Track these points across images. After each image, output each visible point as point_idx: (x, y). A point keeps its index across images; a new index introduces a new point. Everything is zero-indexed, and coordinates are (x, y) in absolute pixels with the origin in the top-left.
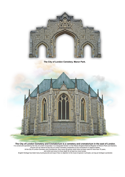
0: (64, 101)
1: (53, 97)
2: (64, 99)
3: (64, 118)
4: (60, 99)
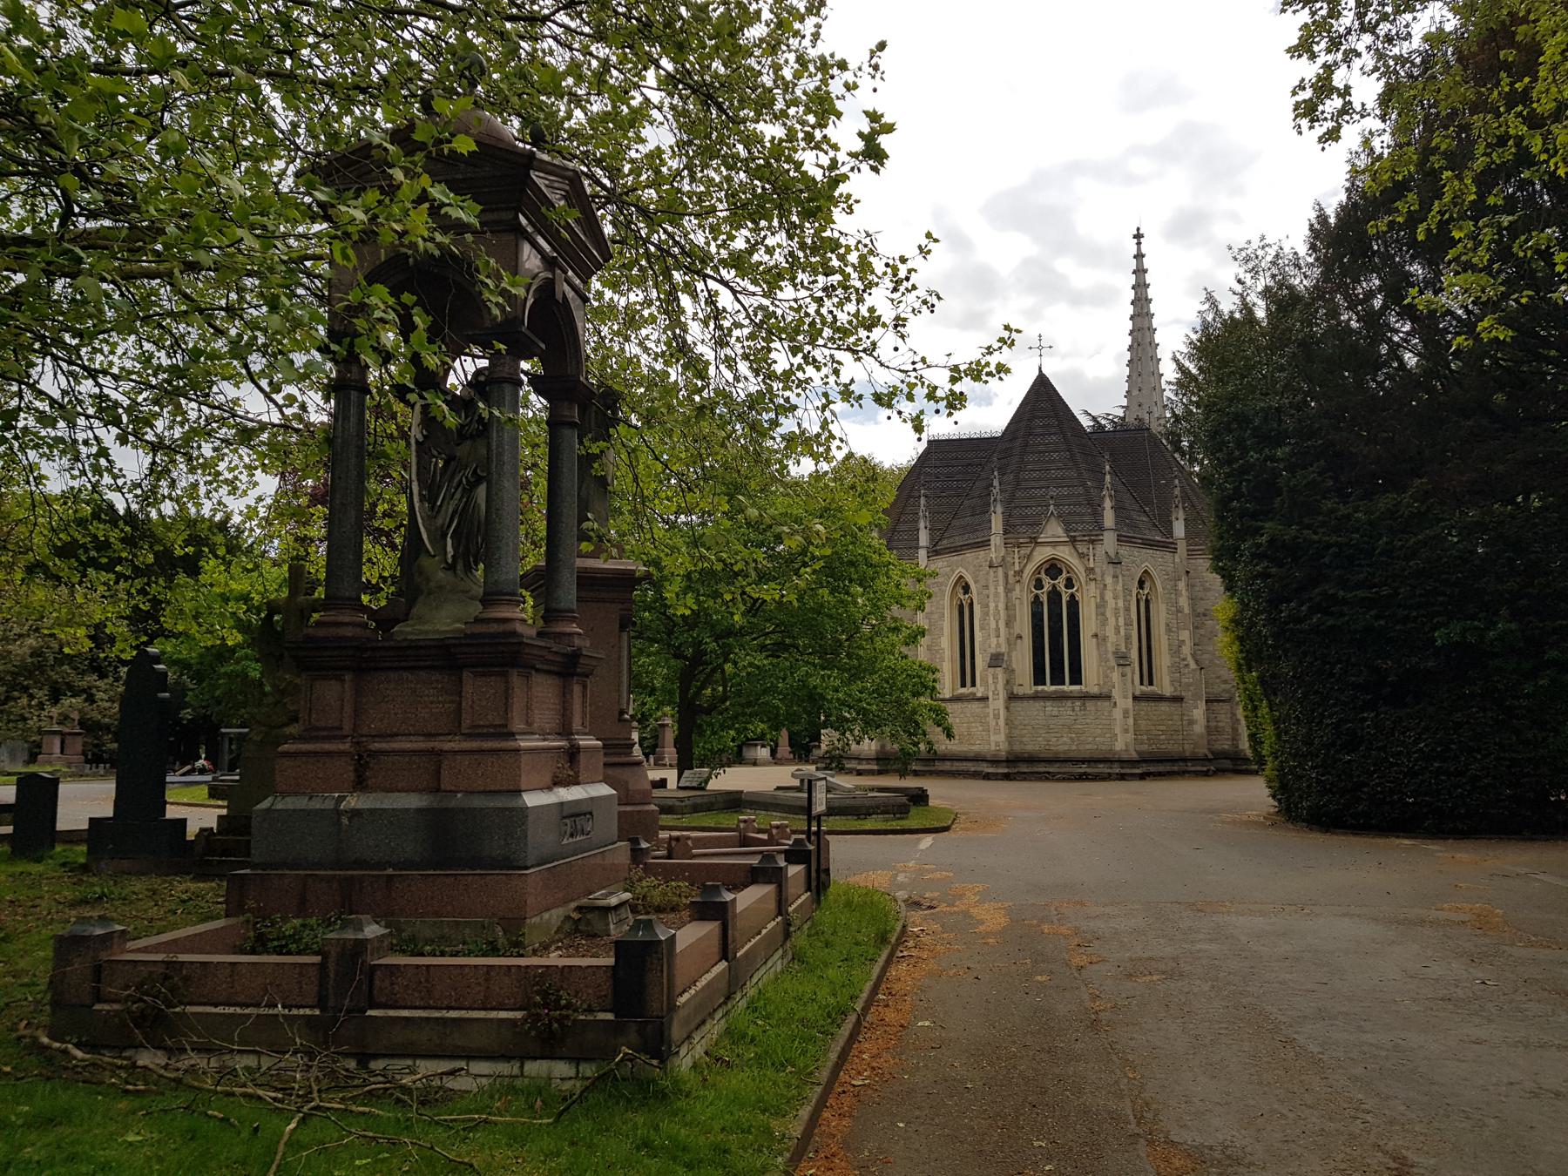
0: (1055, 595)
1: (1006, 576)
2: (1054, 586)
3: (1058, 679)
4: (1039, 585)
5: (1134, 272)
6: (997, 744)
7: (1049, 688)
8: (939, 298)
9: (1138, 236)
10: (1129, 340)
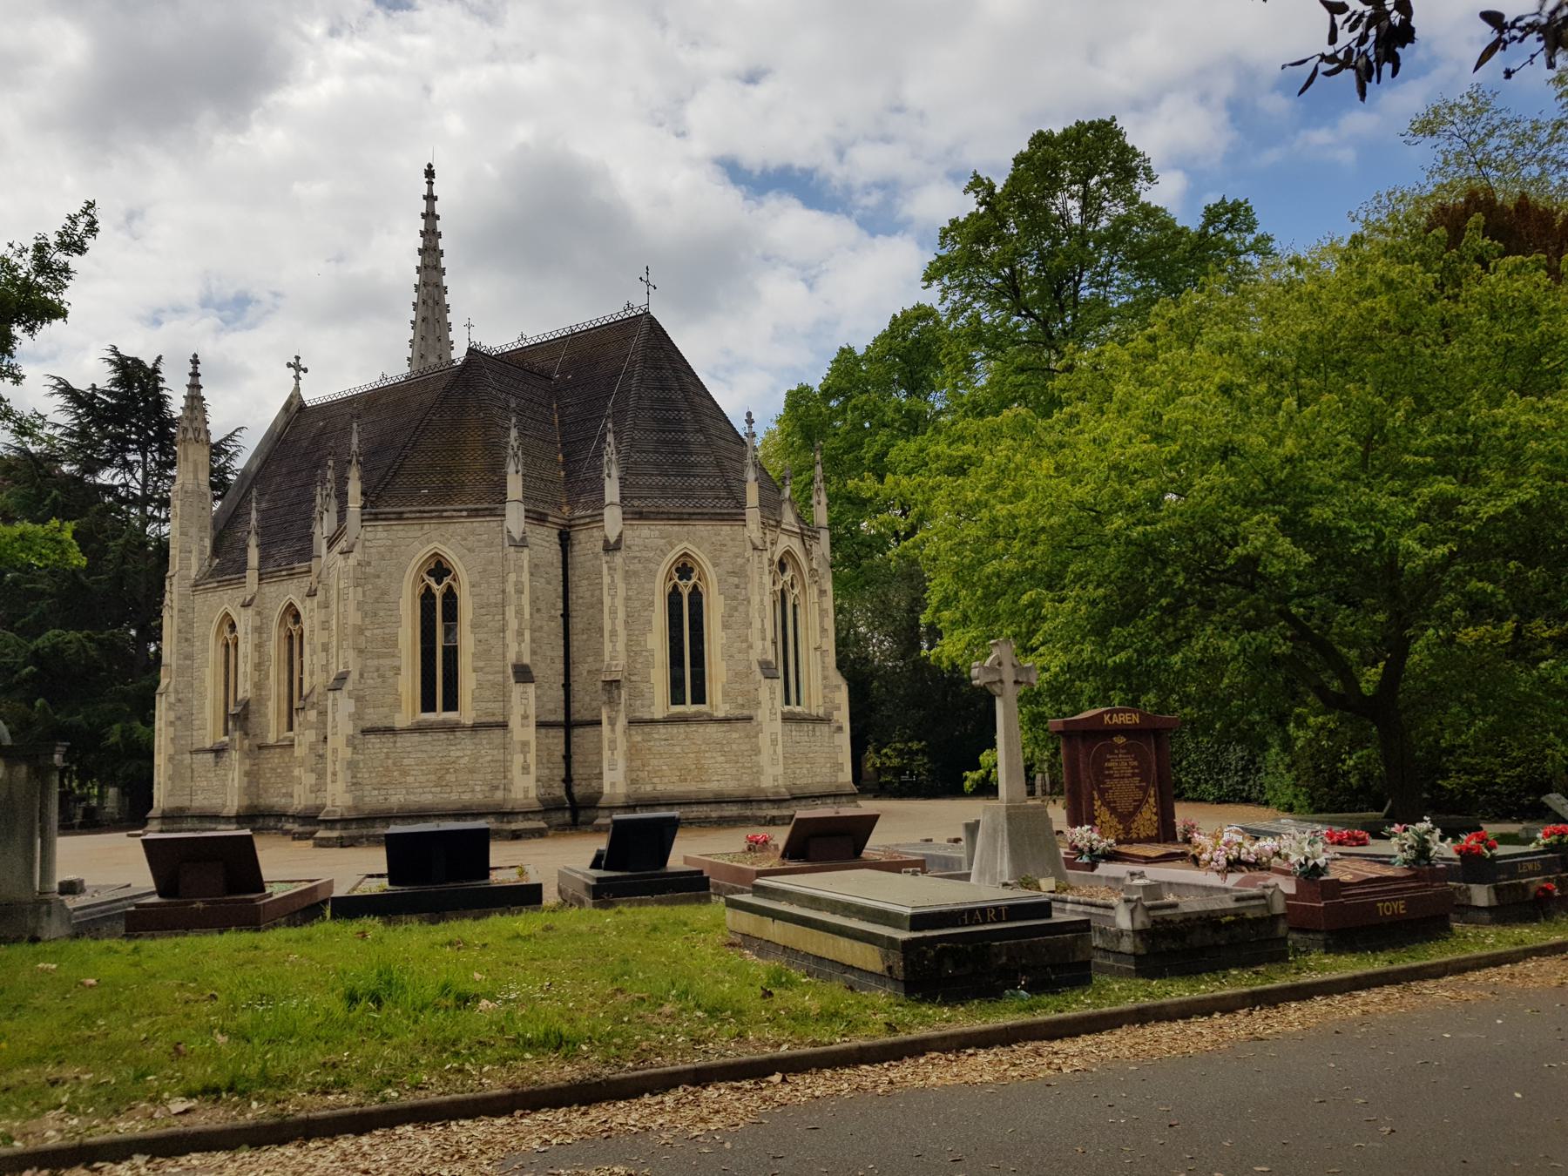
0: (439, 590)
8: (1378, 82)
9: (430, 173)
10: (448, 299)
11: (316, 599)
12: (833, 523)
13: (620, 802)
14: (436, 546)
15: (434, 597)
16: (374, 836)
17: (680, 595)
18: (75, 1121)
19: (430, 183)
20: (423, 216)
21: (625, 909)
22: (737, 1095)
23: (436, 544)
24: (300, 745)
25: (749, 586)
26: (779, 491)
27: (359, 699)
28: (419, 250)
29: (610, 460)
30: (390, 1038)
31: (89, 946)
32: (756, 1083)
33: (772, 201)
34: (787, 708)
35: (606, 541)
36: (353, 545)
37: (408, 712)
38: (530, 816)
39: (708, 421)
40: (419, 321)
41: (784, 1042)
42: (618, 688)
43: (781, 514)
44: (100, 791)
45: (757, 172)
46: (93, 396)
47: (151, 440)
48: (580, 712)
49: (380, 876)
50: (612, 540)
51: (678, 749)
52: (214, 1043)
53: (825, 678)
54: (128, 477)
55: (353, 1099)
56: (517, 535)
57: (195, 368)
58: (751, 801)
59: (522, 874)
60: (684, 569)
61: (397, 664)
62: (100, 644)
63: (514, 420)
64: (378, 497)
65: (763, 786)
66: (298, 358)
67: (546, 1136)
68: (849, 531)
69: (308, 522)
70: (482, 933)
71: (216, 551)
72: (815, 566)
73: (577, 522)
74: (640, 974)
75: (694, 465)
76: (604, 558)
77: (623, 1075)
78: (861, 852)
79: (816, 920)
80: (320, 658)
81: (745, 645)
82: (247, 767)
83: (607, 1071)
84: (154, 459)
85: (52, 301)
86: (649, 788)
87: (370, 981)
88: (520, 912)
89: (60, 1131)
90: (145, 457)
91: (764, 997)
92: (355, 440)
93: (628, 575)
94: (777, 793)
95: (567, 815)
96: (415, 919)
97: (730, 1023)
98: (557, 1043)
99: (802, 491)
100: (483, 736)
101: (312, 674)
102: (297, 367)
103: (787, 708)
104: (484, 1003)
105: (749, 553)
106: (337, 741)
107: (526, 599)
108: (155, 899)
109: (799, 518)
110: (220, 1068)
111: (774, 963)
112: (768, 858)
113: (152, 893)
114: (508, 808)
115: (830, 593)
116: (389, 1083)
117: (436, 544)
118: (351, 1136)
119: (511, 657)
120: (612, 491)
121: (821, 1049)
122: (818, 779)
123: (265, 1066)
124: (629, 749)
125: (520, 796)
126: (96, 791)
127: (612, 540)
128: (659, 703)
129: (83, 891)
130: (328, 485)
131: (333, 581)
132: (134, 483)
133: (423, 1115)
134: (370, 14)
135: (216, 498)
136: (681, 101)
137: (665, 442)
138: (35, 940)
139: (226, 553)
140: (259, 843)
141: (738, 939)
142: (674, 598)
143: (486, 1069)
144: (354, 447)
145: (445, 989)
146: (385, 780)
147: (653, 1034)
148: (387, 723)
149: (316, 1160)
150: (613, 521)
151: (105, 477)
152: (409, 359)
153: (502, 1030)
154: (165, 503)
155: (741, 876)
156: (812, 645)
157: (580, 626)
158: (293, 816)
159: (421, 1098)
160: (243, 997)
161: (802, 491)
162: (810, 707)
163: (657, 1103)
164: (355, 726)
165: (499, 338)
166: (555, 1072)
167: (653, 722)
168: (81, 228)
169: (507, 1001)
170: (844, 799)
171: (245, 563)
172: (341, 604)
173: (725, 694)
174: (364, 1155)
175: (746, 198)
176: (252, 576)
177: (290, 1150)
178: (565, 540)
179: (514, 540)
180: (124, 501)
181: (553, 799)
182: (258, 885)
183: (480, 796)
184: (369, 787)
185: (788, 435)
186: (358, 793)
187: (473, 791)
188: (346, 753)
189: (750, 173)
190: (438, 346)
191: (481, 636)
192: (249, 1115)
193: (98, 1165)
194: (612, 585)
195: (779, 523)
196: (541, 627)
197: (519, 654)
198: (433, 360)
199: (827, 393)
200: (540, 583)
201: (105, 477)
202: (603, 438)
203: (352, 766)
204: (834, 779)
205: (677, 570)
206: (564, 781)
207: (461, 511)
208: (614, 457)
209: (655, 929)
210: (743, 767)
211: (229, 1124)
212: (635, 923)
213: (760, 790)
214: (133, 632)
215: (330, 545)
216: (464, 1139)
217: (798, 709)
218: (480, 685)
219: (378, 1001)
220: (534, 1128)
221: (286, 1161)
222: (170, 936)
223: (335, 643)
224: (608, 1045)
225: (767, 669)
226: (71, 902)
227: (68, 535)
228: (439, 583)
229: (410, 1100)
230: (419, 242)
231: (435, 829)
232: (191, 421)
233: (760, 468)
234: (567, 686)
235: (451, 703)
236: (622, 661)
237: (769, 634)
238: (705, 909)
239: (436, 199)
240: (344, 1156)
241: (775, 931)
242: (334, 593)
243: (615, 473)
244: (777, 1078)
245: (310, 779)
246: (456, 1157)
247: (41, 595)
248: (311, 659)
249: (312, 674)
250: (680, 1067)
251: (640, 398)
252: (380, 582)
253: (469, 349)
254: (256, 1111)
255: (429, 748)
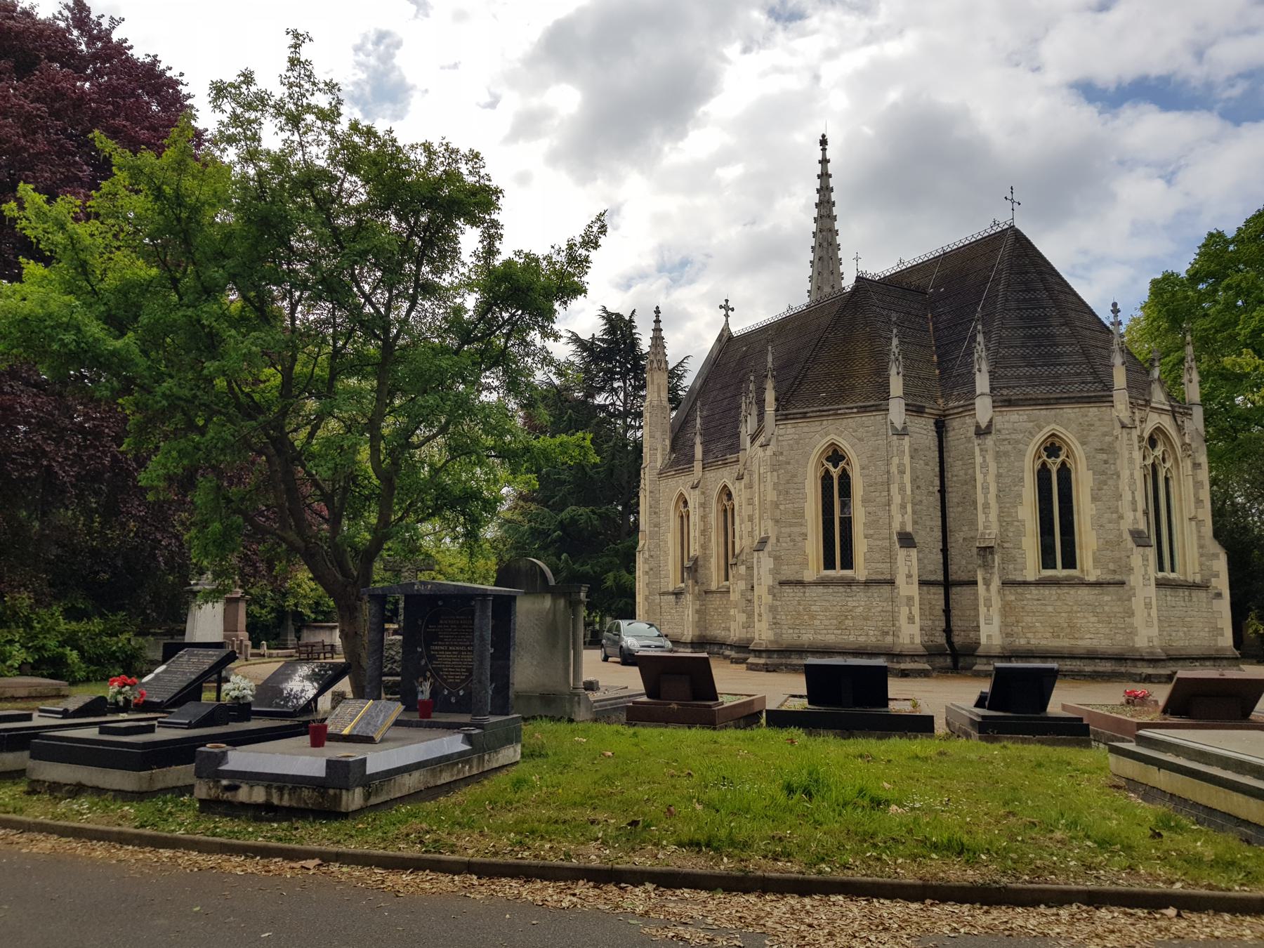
0: (835, 473)
5: (819, 177)
6: (1150, 640)
7: (1060, 572)
9: (824, 142)
10: (839, 240)
11: (743, 482)
12: (1206, 399)
13: (996, 651)
14: (833, 437)
15: (832, 478)
16: (790, 665)
17: (1049, 471)
18: (608, 852)
19: (824, 150)
20: (819, 177)
21: (1009, 745)
22: (1131, 920)
23: (833, 436)
24: (734, 592)
25: (1118, 462)
26: (1148, 373)
27: (777, 559)
28: (816, 204)
29: (980, 357)
30: (821, 824)
31: (605, 729)
32: (1149, 913)
33: (1127, 112)
34: (1160, 575)
35: (978, 427)
36: (770, 440)
37: (813, 569)
38: (916, 659)
39: (1072, 314)
40: (816, 261)
41: (1178, 880)
42: (992, 553)
43: (1150, 394)
44: (601, 619)
45: (1112, 88)
46: (593, 343)
47: (629, 371)
48: (956, 573)
49: (801, 697)
50: (983, 426)
51: (1050, 609)
52: (694, 809)
53: (1201, 547)
54: (615, 398)
55: (797, 868)
56: (899, 426)
57: (657, 316)
58: (1126, 659)
59: (915, 706)
60: (1052, 448)
61: (804, 531)
62: (600, 515)
63: (895, 331)
64: (788, 401)
65: (1137, 646)
66: (727, 301)
67: (955, 925)
68: (1223, 406)
69: (736, 424)
70: (886, 751)
71: (673, 448)
72: (1187, 441)
73: (951, 412)
74: (1029, 802)
75: (1060, 355)
76: (976, 442)
77: (1020, 885)
78: (1250, 714)
79: (1206, 774)
80: (747, 527)
81: (1115, 516)
82: (698, 607)
83: (1005, 880)
84: (631, 385)
85: (576, 283)
86: (1023, 642)
87: (800, 779)
88: (916, 737)
89: (598, 856)
90: (625, 383)
91: (1153, 837)
92: (770, 359)
93: (998, 455)
94: (1152, 653)
95: (949, 660)
96: (830, 733)
97: (1120, 856)
98: (956, 849)
99: (1170, 371)
100: (874, 590)
101: (741, 538)
102: (726, 308)
103: (1160, 575)
104: (894, 807)
105: (1118, 431)
106: (761, 590)
107: (907, 478)
108: (645, 699)
109: (1169, 396)
110: (699, 828)
111: (1161, 808)
112: (1149, 713)
113: (642, 695)
114: (897, 650)
115: (1205, 466)
116: (823, 860)
117: (833, 436)
118: (797, 896)
119: (896, 527)
120: (982, 383)
121: (1217, 893)
122: (1196, 642)
123: (731, 833)
124: (1003, 607)
125: (907, 641)
126: (598, 619)
127: (983, 426)
128: (1031, 567)
129: (598, 689)
130: (751, 395)
131: (755, 468)
132: (618, 403)
133: (852, 890)
134: (772, 29)
135: (673, 409)
136: (1035, 41)
137: (1032, 337)
138: (571, 721)
139: (681, 449)
140: (713, 663)
141: (1123, 783)
142: (1043, 476)
143: (900, 861)
144: (770, 365)
145: (861, 792)
146: (798, 622)
147: (1045, 855)
148: (798, 577)
149: (772, 910)
150: (983, 409)
151: (600, 399)
152: (808, 291)
153: (910, 831)
154: (639, 415)
155: (1119, 725)
156: (1186, 516)
157: (955, 500)
158: (730, 645)
159: (846, 876)
160: (711, 776)
161: (1170, 371)
162: (1185, 573)
163: (1053, 915)
164: (774, 579)
165: (880, 266)
166: (957, 873)
167: (1025, 583)
168: (595, 229)
169: (913, 809)
170: (1225, 662)
171: (693, 456)
172: (762, 485)
173: (1096, 560)
174: (808, 912)
175: (1100, 113)
176: (698, 465)
177: (752, 898)
178: (941, 428)
179: (897, 429)
180: (611, 415)
181: (936, 646)
182: (714, 696)
183: (874, 639)
184: (786, 627)
185: (1154, 320)
186: (778, 631)
187: (867, 635)
188: (767, 599)
189: (1105, 91)
190: (831, 278)
191: (870, 509)
192: (722, 867)
193: (623, 885)
194: (984, 465)
195: (1148, 402)
196: (921, 501)
197: (903, 524)
198: (827, 289)
199: (1195, 277)
200: (920, 464)
201: (600, 399)
202: (973, 338)
203: (773, 609)
204: (1213, 643)
205: (1046, 449)
206: (944, 631)
207: (852, 408)
208: (984, 354)
209: (1040, 765)
210: (1116, 628)
211: (709, 871)
212: (1021, 758)
213: (1134, 649)
214: (620, 508)
215: (753, 440)
216: (885, 915)
217: (1172, 576)
218: (870, 549)
219: (810, 795)
220: (944, 917)
221: (750, 906)
222: (656, 727)
223: (757, 516)
224: (1005, 858)
225: (1139, 538)
226: (593, 696)
227: (588, 442)
228: (835, 466)
229: (841, 876)
230: (816, 198)
231: (843, 663)
232: (656, 355)
233: (1127, 353)
234: (945, 551)
235: (848, 563)
236: (994, 530)
237: (1141, 505)
238: (1087, 752)
239: (829, 161)
240: (793, 911)
241: (1161, 779)
242: (756, 476)
243: (985, 367)
244: (1171, 912)
245: (742, 618)
246: (881, 928)
247: (563, 483)
248: (741, 527)
249: (741, 538)
250: (1073, 887)
251: (1007, 300)
252: (790, 467)
253: (858, 277)
254: (726, 865)
255: (831, 598)
